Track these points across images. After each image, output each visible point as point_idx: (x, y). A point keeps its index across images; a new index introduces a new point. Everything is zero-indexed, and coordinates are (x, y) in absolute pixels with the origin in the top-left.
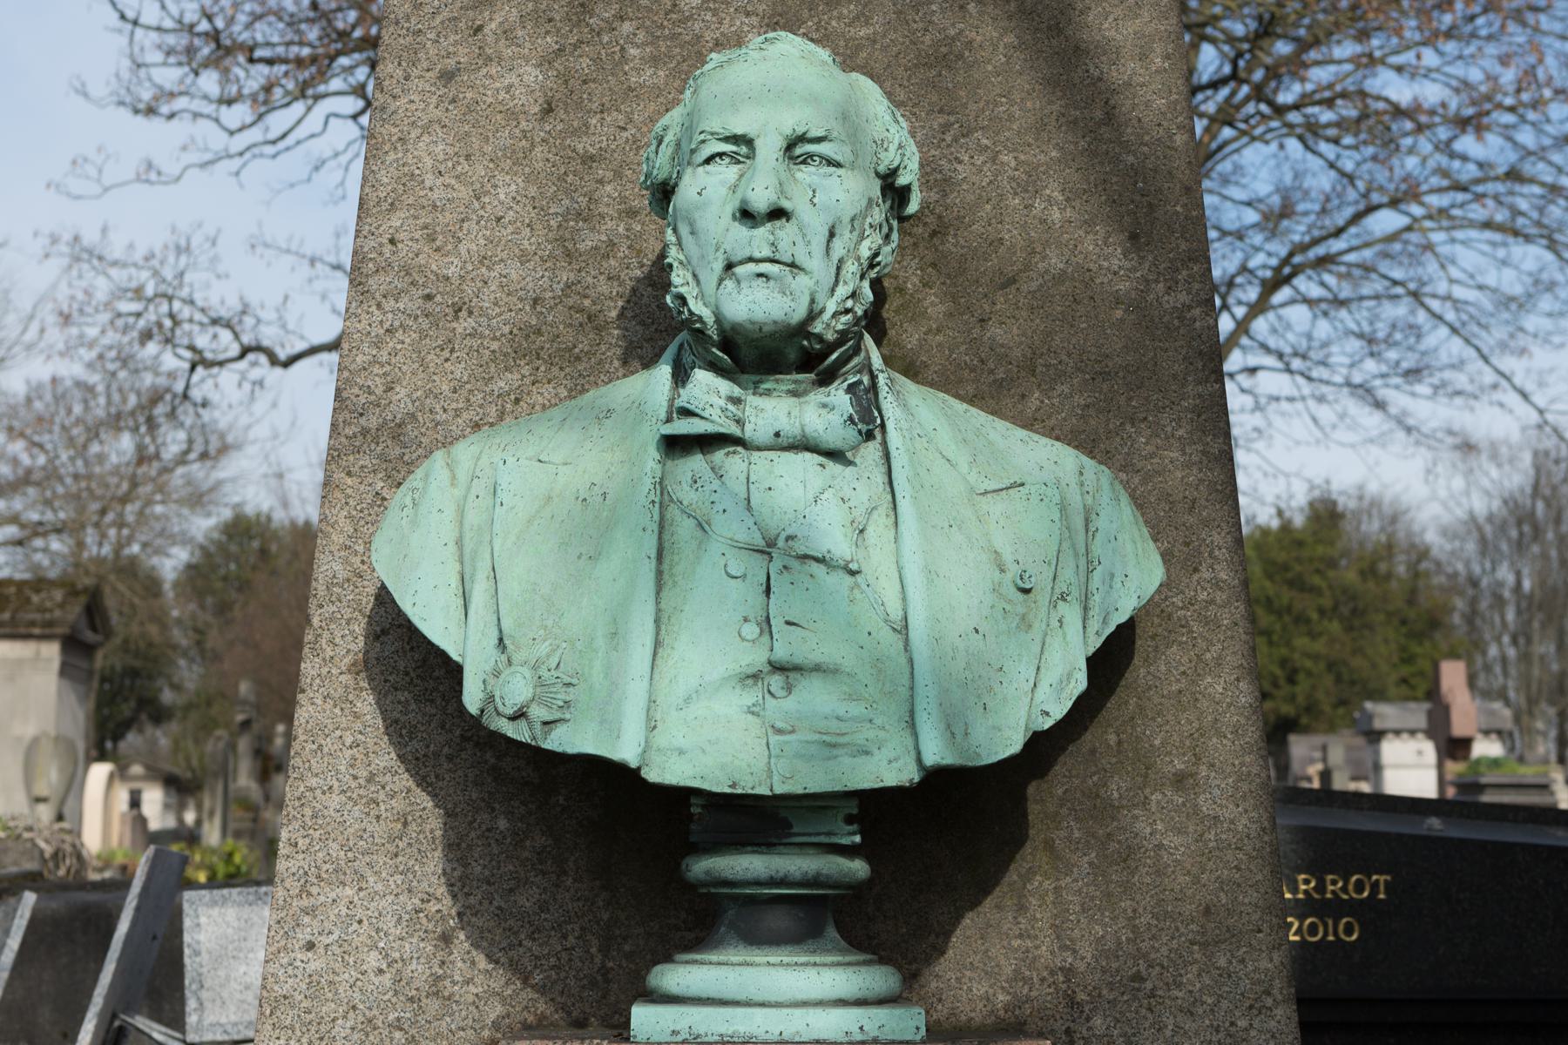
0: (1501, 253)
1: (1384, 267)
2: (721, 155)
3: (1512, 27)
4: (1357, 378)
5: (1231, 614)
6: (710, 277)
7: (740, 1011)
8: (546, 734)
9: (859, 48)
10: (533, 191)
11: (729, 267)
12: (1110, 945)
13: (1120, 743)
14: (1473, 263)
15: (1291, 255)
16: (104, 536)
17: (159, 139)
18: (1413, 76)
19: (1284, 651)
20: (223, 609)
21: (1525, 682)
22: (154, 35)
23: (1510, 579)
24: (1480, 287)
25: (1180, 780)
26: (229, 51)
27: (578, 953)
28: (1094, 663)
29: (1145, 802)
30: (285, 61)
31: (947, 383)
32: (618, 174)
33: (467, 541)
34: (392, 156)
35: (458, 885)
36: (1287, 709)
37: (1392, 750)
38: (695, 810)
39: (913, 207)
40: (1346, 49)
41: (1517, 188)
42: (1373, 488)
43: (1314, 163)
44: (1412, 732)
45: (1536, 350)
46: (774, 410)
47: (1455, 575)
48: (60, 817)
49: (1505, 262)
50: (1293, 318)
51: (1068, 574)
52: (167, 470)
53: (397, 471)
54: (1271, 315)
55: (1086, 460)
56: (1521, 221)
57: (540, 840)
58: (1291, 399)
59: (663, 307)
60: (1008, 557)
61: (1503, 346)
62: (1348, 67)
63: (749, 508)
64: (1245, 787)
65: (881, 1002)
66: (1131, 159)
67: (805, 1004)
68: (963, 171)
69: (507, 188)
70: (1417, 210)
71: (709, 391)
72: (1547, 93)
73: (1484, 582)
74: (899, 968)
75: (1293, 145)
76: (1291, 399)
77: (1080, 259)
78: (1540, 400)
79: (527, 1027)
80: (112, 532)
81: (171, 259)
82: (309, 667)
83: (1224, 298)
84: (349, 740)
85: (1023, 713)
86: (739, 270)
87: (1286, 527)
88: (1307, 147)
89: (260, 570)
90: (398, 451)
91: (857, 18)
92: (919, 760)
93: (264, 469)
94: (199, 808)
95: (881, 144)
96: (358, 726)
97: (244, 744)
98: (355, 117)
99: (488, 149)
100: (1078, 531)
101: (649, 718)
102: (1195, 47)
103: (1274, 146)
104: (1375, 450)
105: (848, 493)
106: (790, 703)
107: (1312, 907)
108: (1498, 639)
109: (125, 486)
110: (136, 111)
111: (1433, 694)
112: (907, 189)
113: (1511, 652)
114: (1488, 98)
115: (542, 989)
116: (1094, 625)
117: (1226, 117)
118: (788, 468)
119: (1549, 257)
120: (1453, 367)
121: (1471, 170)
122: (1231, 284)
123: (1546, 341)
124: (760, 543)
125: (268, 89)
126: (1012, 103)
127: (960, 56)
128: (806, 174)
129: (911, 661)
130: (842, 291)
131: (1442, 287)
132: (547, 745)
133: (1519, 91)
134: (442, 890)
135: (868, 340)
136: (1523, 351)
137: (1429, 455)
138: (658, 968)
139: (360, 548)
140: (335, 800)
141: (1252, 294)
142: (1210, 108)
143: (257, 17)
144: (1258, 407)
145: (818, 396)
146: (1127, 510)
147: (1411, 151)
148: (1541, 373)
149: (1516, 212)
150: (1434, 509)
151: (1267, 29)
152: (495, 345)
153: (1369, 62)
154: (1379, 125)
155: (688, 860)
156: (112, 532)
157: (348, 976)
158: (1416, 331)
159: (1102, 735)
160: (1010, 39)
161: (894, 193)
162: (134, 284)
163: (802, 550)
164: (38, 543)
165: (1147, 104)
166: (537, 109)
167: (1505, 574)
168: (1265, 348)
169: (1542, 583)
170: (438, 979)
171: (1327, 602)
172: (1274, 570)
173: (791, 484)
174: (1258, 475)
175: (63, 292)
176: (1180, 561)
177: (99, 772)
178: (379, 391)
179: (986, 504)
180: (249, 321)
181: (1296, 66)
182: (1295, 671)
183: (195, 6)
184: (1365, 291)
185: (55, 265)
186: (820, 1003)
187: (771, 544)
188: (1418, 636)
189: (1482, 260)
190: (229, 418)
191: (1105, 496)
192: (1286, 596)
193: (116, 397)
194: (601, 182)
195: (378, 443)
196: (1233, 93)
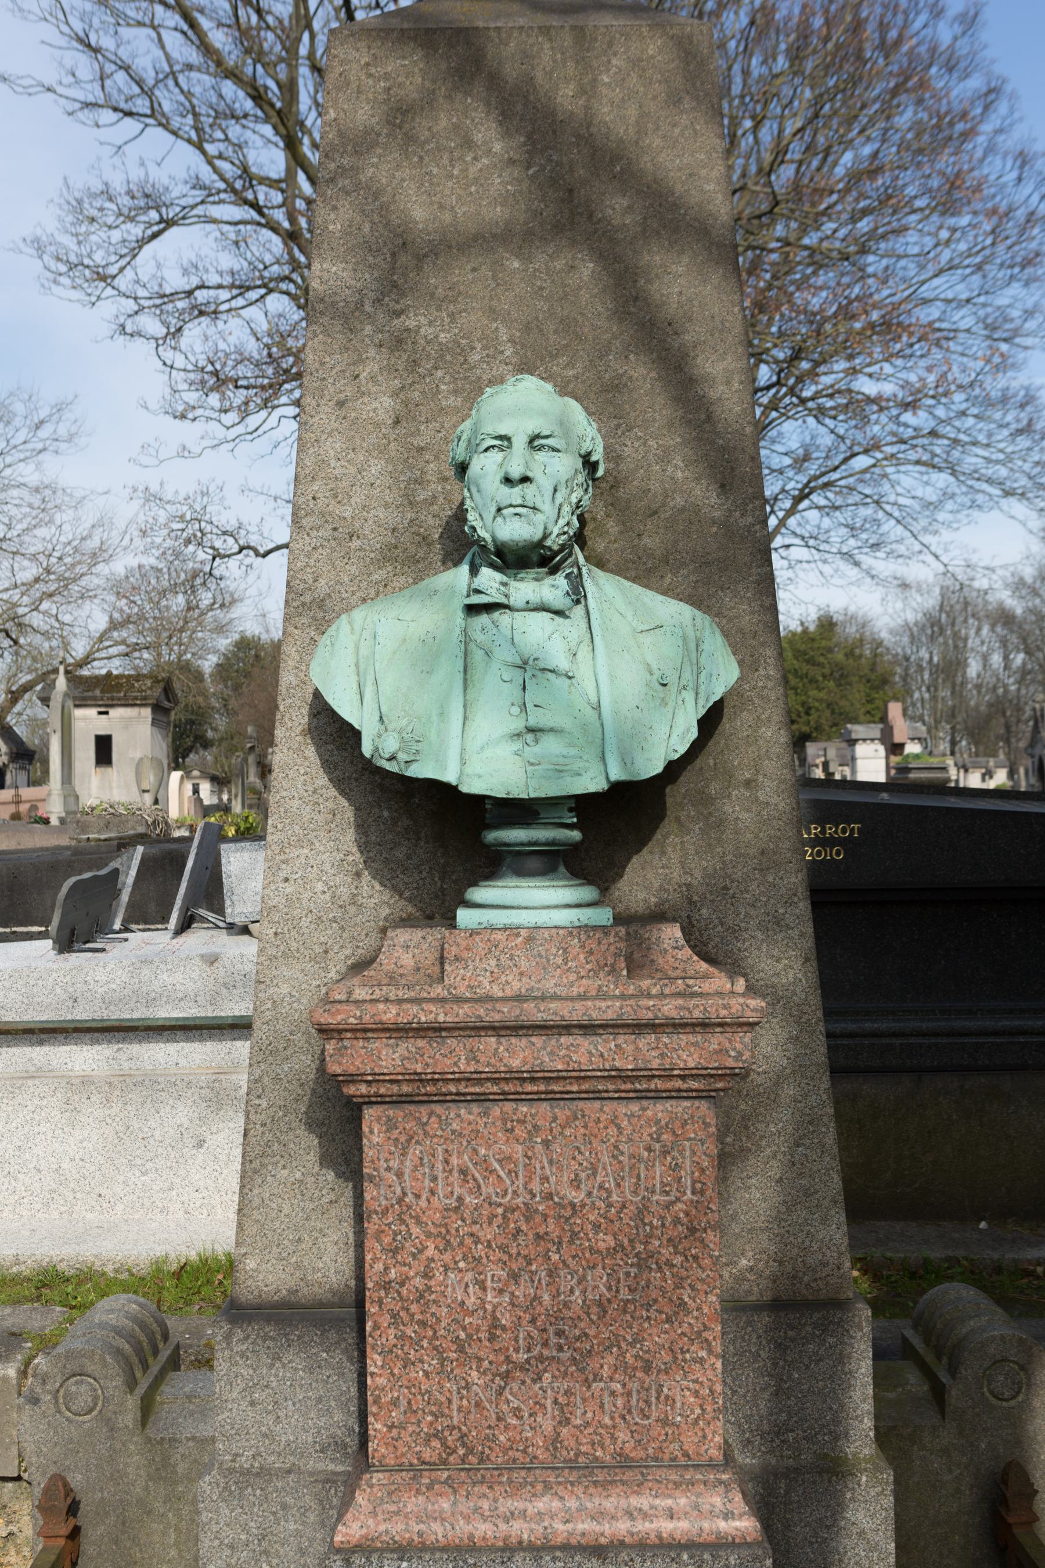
0: (925, 478)
1: (861, 487)
2: (493, 447)
3: (934, 350)
4: (845, 550)
5: (775, 693)
6: (489, 516)
7: (514, 911)
8: (407, 768)
9: (569, 382)
10: (390, 468)
11: (499, 510)
12: (711, 871)
14: (910, 484)
15: (809, 482)
16: (171, 650)
17: (188, 432)
18: (878, 379)
19: (804, 698)
20: (237, 688)
21: (934, 709)
22: (182, 374)
23: (927, 656)
24: (913, 498)
25: (748, 783)
26: (224, 382)
27: (428, 881)
29: (729, 795)
30: (254, 387)
31: (619, 571)
32: (437, 457)
33: (361, 661)
34: (311, 450)
35: (364, 847)
36: (805, 729)
37: (862, 750)
38: (488, 806)
39: (600, 473)
40: (841, 365)
41: (935, 441)
42: (852, 609)
43: (823, 430)
44: (872, 740)
45: (943, 531)
46: (526, 588)
47: (897, 654)
48: (156, 802)
49: (927, 483)
50: (810, 518)
51: (687, 675)
52: (202, 614)
53: (322, 626)
54: (798, 516)
55: (696, 612)
56: (936, 460)
57: (406, 822)
58: (809, 562)
59: (463, 531)
60: (654, 667)
61: (925, 530)
62: (842, 375)
63: (513, 643)
64: (783, 786)
65: (589, 905)
66: (721, 442)
67: (548, 907)
68: (627, 451)
69: (376, 467)
70: (879, 455)
71: (489, 579)
72: (953, 388)
73: (912, 659)
74: (598, 886)
75: (811, 420)
76: (809, 562)
77: (693, 499)
78: (945, 559)
79: (402, 920)
80: (176, 648)
81: (199, 499)
82: (279, 733)
83: (772, 507)
84: (302, 771)
85: (663, 751)
86: (504, 512)
87: (805, 631)
88: (819, 422)
89: (254, 666)
92: (607, 778)
93: (255, 612)
94: (230, 792)
95: (582, 438)
96: (307, 763)
97: (251, 759)
98: (295, 418)
99: (365, 445)
100: (692, 651)
101: (462, 758)
102: (757, 365)
103: (800, 421)
104: (854, 589)
105: (566, 634)
106: (537, 749)
107: (818, 841)
108: (919, 689)
109: (181, 623)
110: (175, 417)
111: (884, 719)
112: (597, 463)
113: (927, 696)
114: (919, 391)
115: (409, 900)
116: (701, 702)
117: (773, 405)
118: (533, 618)
119: (952, 479)
120: (897, 541)
121: (910, 432)
122: (776, 499)
123: (949, 527)
124: (519, 662)
125: (246, 403)
126: (655, 411)
127: (625, 385)
128: (541, 457)
129: (602, 725)
131: (892, 498)
132: (408, 774)
133: (937, 387)
134: (355, 849)
135: (576, 548)
136: (936, 532)
137: (883, 590)
138: (470, 890)
139: (304, 668)
140: (296, 803)
141: (788, 504)
142: (765, 400)
143: (238, 362)
144: (790, 567)
145: (549, 580)
146: (719, 638)
147: (877, 422)
148: (946, 544)
149: (934, 455)
150: (886, 619)
151: (797, 356)
152: (372, 555)
153: (854, 372)
154: (858, 407)
155: (485, 833)
156: (176, 648)
157: (307, 895)
158: (877, 522)
159: (706, 760)
160: (653, 374)
161: (589, 465)
162: (179, 514)
163: (542, 666)
164: (137, 654)
165: (730, 410)
166: (390, 421)
167: (924, 654)
168: (794, 533)
169: (944, 658)
170: (354, 895)
171: (827, 671)
172: (798, 654)
173: (536, 632)
174: (790, 604)
175: (141, 519)
176: (748, 664)
177: (176, 776)
178: (310, 582)
179: (642, 638)
180: (243, 532)
181: (813, 374)
182: (810, 708)
183: (204, 357)
184: (850, 501)
185: (136, 504)
186: (556, 907)
187: (526, 663)
188: (876, 688)
189: (915, 483)
190: (235, 584)
191: (707, 632)
192: (805, 668)
193: (174, 574)
194: (427, 462)
195: (311, 610)
196: (778, 392)
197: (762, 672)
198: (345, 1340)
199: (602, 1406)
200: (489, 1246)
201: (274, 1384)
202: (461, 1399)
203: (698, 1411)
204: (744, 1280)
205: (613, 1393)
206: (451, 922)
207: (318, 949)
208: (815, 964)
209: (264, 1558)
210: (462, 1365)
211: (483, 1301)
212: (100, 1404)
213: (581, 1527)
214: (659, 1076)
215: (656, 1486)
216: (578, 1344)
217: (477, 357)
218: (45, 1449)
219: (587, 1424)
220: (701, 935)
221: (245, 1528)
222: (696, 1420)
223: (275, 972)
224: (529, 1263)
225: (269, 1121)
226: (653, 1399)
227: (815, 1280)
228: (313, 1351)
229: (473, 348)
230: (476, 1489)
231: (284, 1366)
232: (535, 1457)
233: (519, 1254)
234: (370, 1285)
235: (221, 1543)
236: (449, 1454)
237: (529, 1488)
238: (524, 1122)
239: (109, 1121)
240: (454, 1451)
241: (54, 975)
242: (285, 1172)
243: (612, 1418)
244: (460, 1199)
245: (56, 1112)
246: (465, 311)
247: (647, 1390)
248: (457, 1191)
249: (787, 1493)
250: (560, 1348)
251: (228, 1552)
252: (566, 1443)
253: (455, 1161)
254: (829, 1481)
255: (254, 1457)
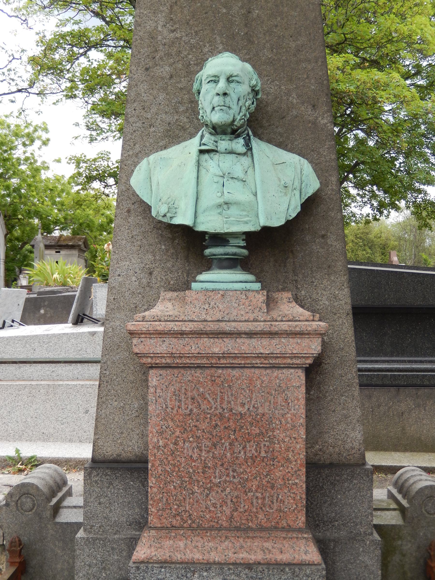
2: (212, 81)
10: (168, 97)
13: (309, 228)
25: (323, 236)
28: (302, 205)
34: (134, 89)
55: (301, 158)
57: (172, 251)
84: (127, 228)
90: (137, 160)
91: (246, 54)
124: (222, 175)
128: (233, 85)
130: (241, 114)
140: (124, 242)
152: (160, 134)
166: (168, 77)
170: (149, 283)
178: (132, 146)
194: (184, 94)
197: (330, 188)
198: (141, 476)
199: (252, 503)
200: (204, 431)
201: (109, 495)
202: (190, 498)
203: (295, 506)
204: (317, 454)
205: (257, 498)
206: (189, 288)
207: (133, 306)
208: (351, 316)
209: (103, 571)
210: (190, 483)
211: (200, 456)
212: (36, 507)
213: (241, 556)
214: (280, 357)
215: (275, 539)
216: (242, 476)
217: (207, 50)
218: (11, 526)
219: (246, 511)
220: (301, 302)
221: (95, 558)
222: (294, 511)
223: (113, 316)
224: (221, 440)
225: (109, 381)
226: (275, 501)
227: (349, 455)
228: (127, 481)
229: (205, 46)
230: (196, 538)
231: (114, 488)
232: (222, 525)
233: (216, 435)
234: (151, 447)
235: (85, 564)
236: (184, 523)
237: (219, 538)
238: (220, 377)
239: (48, 401)
240: (186, 522)
241: (26, 339)
242: (116, 403)
243: (257, 509)
244: (191, 410)
245: (25, 397)
246: (201, 30)
247: (272, 497)
248: (190, 407)
249: (334, 548)
250: (234, 477)
251: (87, 568)
252: (236, 519)
253: (189, 394)
254: (353, 543)
255: (100, 527)
